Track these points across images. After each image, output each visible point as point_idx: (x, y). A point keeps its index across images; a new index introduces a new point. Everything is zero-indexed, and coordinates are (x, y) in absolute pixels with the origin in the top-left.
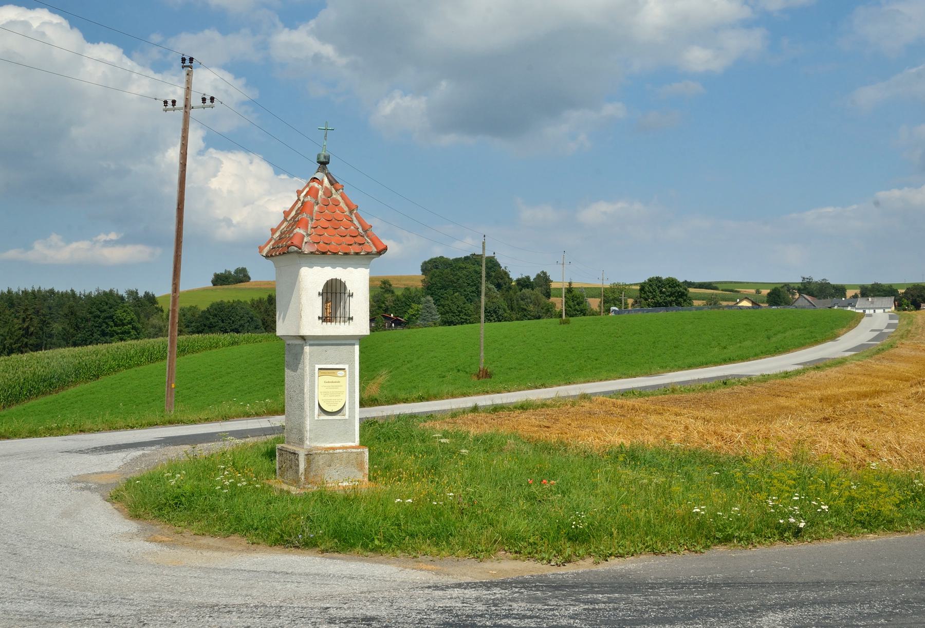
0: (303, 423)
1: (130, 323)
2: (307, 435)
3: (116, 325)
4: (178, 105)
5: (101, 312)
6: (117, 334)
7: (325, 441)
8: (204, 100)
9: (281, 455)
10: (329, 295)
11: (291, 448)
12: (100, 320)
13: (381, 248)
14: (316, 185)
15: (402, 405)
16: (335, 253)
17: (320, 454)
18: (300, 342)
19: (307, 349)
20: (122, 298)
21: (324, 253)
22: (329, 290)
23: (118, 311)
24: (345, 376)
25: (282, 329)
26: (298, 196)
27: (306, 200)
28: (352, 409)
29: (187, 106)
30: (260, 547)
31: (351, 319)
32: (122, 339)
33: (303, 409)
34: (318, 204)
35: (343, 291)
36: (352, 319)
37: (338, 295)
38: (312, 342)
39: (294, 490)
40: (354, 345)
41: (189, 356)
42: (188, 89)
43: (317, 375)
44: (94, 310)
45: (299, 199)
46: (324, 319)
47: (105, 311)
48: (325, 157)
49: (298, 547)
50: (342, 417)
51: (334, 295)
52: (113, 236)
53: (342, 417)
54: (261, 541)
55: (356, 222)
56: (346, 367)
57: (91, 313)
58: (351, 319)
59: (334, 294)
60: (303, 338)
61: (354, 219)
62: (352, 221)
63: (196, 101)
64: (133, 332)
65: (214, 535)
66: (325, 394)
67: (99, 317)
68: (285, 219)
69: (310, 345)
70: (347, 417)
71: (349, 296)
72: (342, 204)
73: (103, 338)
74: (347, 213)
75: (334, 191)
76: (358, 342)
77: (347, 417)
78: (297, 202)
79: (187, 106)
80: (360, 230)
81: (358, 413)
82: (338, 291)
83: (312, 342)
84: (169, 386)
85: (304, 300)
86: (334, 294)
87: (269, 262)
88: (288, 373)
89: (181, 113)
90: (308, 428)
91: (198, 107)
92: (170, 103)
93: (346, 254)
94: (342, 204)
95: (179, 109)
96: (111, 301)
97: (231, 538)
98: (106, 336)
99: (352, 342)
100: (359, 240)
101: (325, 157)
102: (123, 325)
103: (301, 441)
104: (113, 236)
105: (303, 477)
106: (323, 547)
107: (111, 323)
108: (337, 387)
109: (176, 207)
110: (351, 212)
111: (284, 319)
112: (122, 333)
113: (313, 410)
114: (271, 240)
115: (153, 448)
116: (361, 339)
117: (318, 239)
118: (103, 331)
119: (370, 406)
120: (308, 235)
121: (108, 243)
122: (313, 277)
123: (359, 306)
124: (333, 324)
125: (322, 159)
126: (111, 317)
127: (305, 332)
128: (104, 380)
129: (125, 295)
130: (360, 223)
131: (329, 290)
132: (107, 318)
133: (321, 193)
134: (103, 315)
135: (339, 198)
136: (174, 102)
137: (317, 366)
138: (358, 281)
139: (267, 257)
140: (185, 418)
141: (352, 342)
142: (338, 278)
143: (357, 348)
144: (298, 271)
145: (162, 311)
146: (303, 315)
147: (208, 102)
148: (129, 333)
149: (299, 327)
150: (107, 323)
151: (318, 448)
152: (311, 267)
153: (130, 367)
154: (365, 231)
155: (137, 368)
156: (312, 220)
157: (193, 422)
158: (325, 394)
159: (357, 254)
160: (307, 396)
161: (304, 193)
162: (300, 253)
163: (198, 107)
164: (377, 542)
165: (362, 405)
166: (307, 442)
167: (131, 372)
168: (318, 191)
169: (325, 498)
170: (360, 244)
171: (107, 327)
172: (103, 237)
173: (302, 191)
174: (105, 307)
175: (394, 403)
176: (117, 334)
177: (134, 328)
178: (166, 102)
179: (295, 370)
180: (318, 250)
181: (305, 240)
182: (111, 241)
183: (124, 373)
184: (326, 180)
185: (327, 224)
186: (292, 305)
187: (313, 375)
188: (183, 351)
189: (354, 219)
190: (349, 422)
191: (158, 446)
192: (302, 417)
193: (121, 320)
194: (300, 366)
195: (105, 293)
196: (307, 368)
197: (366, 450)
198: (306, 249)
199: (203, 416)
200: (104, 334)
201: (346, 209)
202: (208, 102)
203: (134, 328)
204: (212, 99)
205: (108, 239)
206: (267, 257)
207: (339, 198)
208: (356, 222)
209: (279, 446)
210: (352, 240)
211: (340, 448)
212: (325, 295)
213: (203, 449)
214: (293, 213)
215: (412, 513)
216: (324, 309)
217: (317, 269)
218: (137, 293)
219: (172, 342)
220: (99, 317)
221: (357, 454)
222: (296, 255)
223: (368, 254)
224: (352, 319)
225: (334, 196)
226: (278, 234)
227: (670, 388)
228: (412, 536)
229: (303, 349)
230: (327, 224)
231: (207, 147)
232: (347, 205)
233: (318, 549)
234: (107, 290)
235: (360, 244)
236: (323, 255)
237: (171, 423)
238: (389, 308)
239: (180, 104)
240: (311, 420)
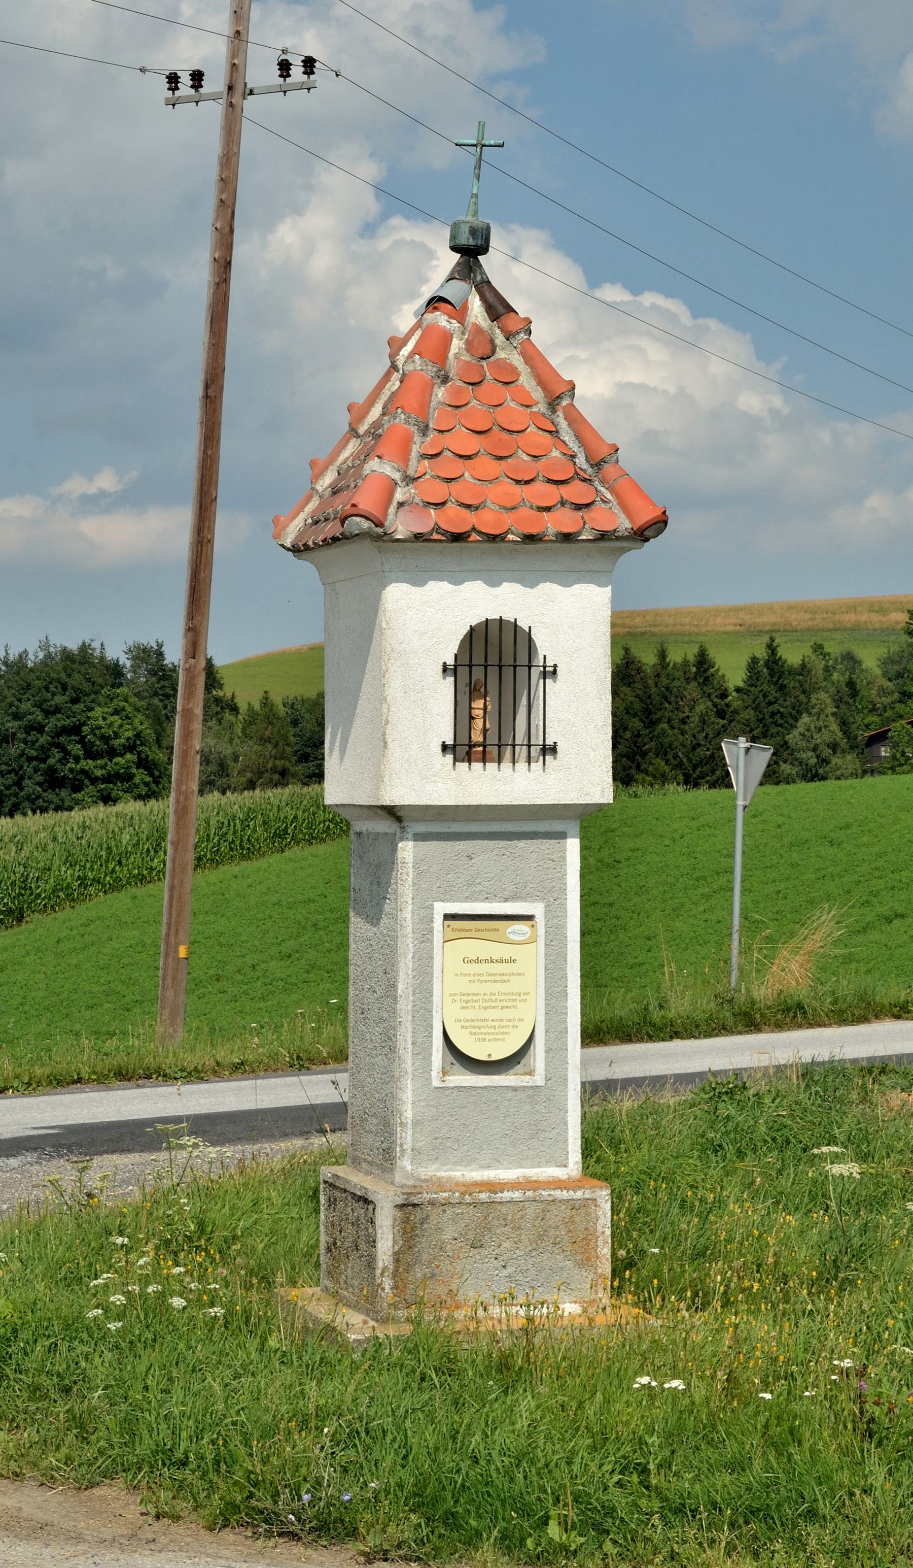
0: (394, 1097)
1: (130, 748)
2: (407, 1137)
3: (90, 754)
4: (208, 87)
5: (47, 713)
6: (94, 781)
7: (466, 1161)
8: (285, 67)
9: (332, 1202)
10: (478, 673)
11: (356, 1179)
12: (43, 740)
13: (646, 516)
14: (441, 319)
15: (888, 1026)
16: (493, 538)
17: (447, 1204)
18: (385, 826)
19: (407, 850)
20: (115, 670)
21: (458, 538)
22: (478, 659)
23: (98, 711)
24: (533, 940)
25: (339, 787)
26: (393, 356)
27: (410, 367)
28: (556, 1052)
29: (236, 89)
30: (178, 1529)
31: (549, 750)
32: (107, 799)
33: (393, 1049)
34: (445, 379)
35: (522, 659)
36: (553, 750)
37: (508, 672)
38: (421, 828)
39: (356, 1326)
40: (563, 836)
41: (295, 852)
42: (238, 36)
43: (438, 936)
44: (25, 706)
45: (394, 367)
46: (462, 750)
47: (57, 710)
48: (473, 232)
49: (293, 1536)
50: (525, 1081)
51: (493, 672)
52: (106, 481)
53: (525, 1081)
54: (183, 1506)
55: (567, 436)
56: (536, 909)
57: (16, 716)
58: (549, 750)
59: (494, 664)
60: (392, 812)
61: (563, 424)
62: (554, 433)
63: (261, 71)
64: (140, 776)
65: (48, 1480)
66: (468, 1000)
67: (40, 729)
68: (353, 432)
69: (419, 837)
70: (539, 1079)
71: (544, 675)
72: (526, 380)
73: (50, 795)
74: (542, 407)
75: (500, 338)
76: (574, 827)
77: (539, 1079)
78: (387, 377)
79: (236, 89)
80: (581, 461)
81: (577, 1063)
82: (508, 660)
83: (421, 828)
84: (171, 951)
85: (394, 688)
86: (494, 664)
87: (305, 568)
88: (357, 926)
89: (214, 111)
90: (408, 1114)
91: (269, 91)
92: (185, 80)
93: (530, 538)
94: (526, 380)
95: (214, 98)
96: (76, 680)
97: (97, 1492)
98: (59, 787)
99: (558, 827)
100: (576, 492)
101: (473, 232)
102: (112, 753)
103: (386, 1159)
104: (106, 481)
105: (387, 1284)
106: (372, 1541)
107: (77, 749)
108: (504, 978)
109: (199, 391)
110: (553, 403)
111: (343, 751)
112: (110, 778)
113: (423, 1052)
114: (309, 499)
115: (13, 1162)
116: (586, 818)
117: (439, 492)
118: (51, 772)
119: (779, 1026)
120: (410, 480)
121: (94, 504)
122: (426, 619)
123: (578, 711)
124: (492, 766)
125: (465, 239)
126: (75, 730)
127: (400, 792)
128: (39, 926)
129: (125, 661)
130: (579, 437)
131: (478, 659)
132: (64, 731)
133: (457, 345)
134: (53, 723)
135: (517, 360)
136: (197, 77)
137: (441, 908)
138: (572, 625)
139: (296, 550)
140: (168, 1062)
141: (558, 827)
142: (509, 616)
143: (573, 846)
144: (377, 599)
145: (235, 709)
146: (398, 744)
147: (297, 72)
148: (129, 777)
149: (378, 778)
150: (63, 749)
151: (439, 1184)
152: (419, 582)
153: (117, 886)
154: (597, 465)
155: (140, 891)
156: (424, 430)
157: (195, 1075)
158: (468, 1000)
159: (567, 538)
160: (405, 1006)
161: (410, 346)
162: (380, 537)
163: (269, 91)
164: (554, 1530)
165: (593, 1035)
166: (406, 1164)
167: (121, 900)
168: (447, 338)
169: (433, 1363)
170: (578, 507)
171: (63, 761)
172: (76, 486)
173: (404, 342)
174: (59, 699)
175: (863, 1019)
176: (94, 781)
177: (144, 763)
178: (173, 80)
179: (374, 919)
180: (437, 529)
181: (399, 496)
182: (103, 494)
183: (101, 905)
184: (476, 305)
185: (471, 444)
186: (363, 707)
187: (425, 936)
188: (281, 835)
189: (563, 424)
190: (547, 1097)
191: (30, 1157)
192: (390, 1078)
193: (105, 739)
194: (387, 908)
195: (67, 655)
196: (407, 915)
197: (603, 1196)
198: (401, 526)
199: (226, 1054)
200: (53, 781)
201: (537, 394)
202: (297, 72)
203: (144, 763)
204: (309, 64)
205: (93, 490)
206: (296, 550)
207: (517, 360)
208: (567, 436)
209: (327, 1172)
210: (552, 494)
211: (514, 1186)
212: (463, 672)
213: (116, 1178)
214: (376, 412)
215: (691, 1430)
216: (462, 717)
217: (437, 589)
218: (160, 655)
219: (182, 812)
220: (40, 729)
221: (573, 1205)
222: (367, 546)
223: (603, 536)
224: (553, 750)
225: (501, 354)
226: (329, 478)
227: (878, 1064)
228: (680, 1510)
229: (394, 850)
230: (471, 444)
231: (384, 216)
232: (541, 383)
233: (355, 1547)
234: (73, 646)
235: (578, 507)
236: (455, 546)
237: (124, 1076)
238: (665, 718)
239: (214, 83)
240: (418, 1086)
